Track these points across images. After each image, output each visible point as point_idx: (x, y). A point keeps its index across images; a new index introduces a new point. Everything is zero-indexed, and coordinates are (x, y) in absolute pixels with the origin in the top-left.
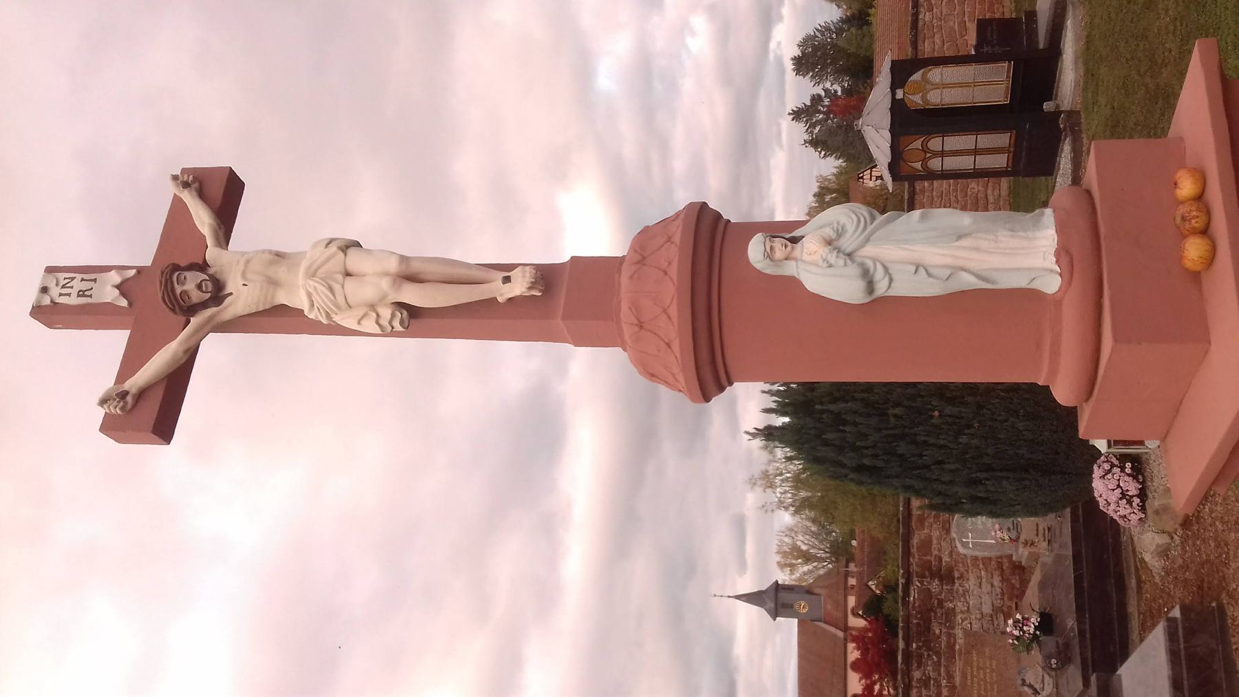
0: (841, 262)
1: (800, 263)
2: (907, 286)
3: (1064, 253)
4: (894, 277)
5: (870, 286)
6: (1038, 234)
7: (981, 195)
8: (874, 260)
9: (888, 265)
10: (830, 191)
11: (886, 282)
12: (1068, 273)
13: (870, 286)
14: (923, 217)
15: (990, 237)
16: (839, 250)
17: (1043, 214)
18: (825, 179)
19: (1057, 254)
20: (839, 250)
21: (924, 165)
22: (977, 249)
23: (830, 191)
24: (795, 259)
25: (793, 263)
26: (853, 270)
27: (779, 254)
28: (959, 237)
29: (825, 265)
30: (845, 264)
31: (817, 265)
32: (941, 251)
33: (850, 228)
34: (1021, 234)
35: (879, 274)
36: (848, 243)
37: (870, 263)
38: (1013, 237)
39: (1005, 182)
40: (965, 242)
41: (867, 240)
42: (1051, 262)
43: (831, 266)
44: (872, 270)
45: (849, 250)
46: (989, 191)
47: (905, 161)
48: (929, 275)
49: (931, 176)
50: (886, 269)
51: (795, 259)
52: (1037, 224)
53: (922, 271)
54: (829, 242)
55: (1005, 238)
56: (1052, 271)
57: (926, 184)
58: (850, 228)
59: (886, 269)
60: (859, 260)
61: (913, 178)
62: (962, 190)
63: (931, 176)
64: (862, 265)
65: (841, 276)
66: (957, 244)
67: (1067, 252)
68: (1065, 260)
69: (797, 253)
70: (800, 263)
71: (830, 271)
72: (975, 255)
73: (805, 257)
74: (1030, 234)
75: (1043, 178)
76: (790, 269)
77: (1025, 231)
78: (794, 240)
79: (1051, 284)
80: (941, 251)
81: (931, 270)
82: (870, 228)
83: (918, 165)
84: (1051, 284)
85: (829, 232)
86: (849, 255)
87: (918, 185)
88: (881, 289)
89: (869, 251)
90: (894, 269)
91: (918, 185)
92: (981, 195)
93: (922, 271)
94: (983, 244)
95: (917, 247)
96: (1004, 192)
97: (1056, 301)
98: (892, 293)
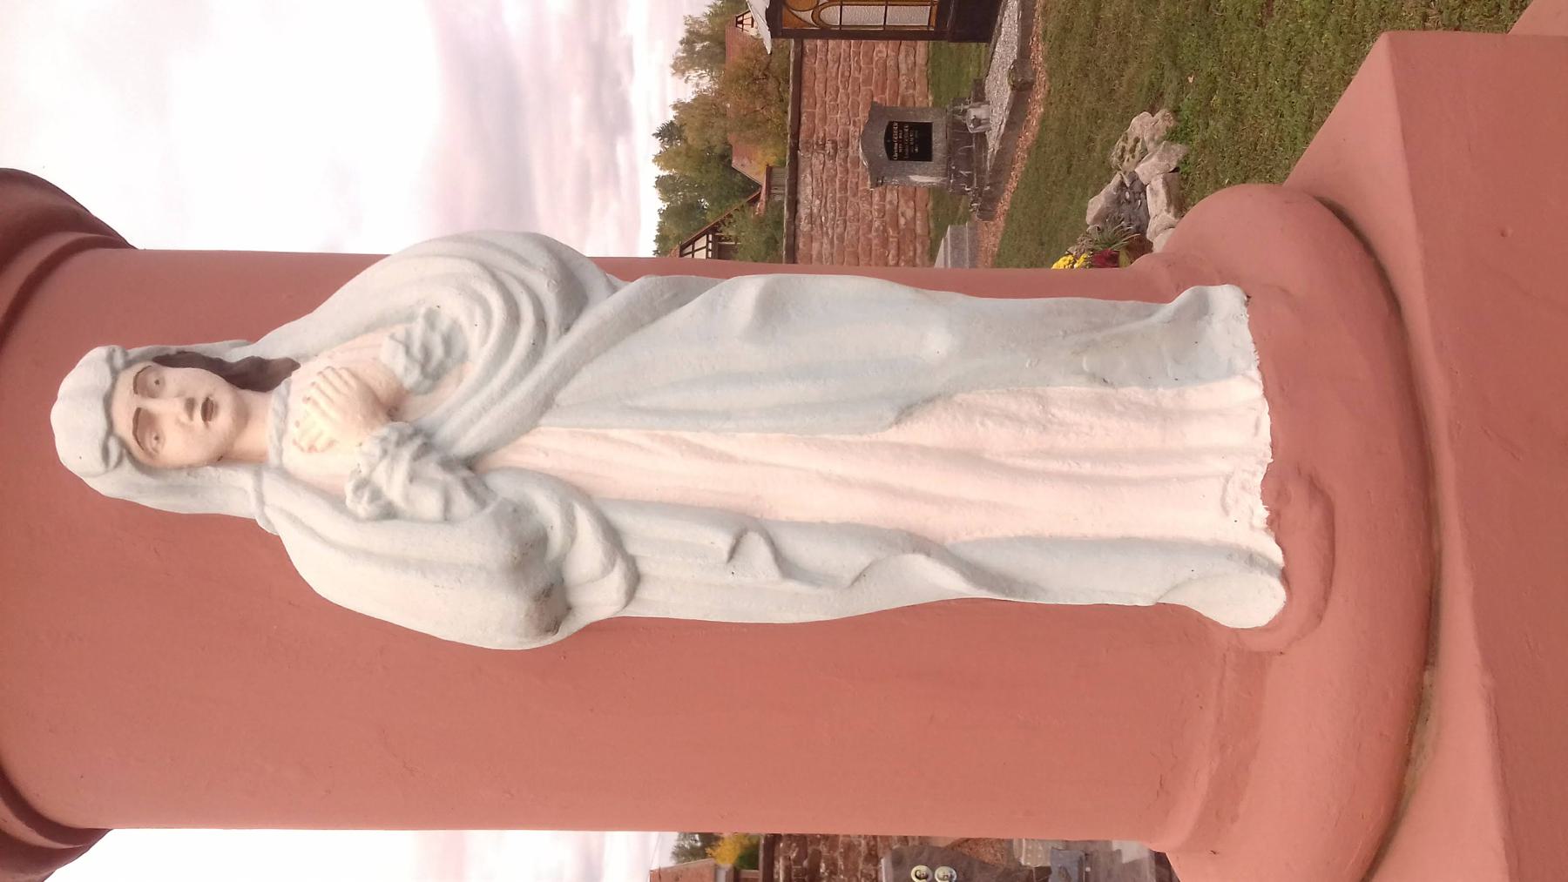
0: (429, 503)
1: (270, 482)
2: (691, 584)
3: (1295, 485)
4: (644, 567)
5: (552, 600)
6: (1197, 396)
7: (890, 63)
8: (572, 492)
9: (624, 520)
10: (702, 38)
11: (616, 580)
12: (1315, 567)
13: (552, 600)
14: (769, 310)
15: (1028, 407)
16: (426, 443)
17: (1202, 309)
18: (696, 21)
19: (1276, 490)
20: (426, 443)
21: (816, 16)
22: (970, 459)
23: (702, 38)
24: (256, 462)
25: (242, 479)
26: (478, 543)
27: (179, 439)
28: (906, 411)
29: (363, 507)
30: (447, 516)
31: (334, 500)
32: (838, 467)
33: (479, 345)
34: (1135, 392)
35: (586, 557)
36: (463, 415)
37: (548, 509)
38: (1103, 405)
39: (921, 46)
40: (925, 431)
41: (544, 404)
42: (1247, 521)
43: (389, 513)
44: (557, 538)
45: (467, 444)
46: (901, 57)
47: (788, 7)
48: (785, 565)
49: (826, 32)
50: (613, 537)
51: (256, 462)
52: (1186, 354)
53: (758, 550)
54: (389, 407)
55: (1079, 417)
56: (1252, 559)
57: (819, 42)
58: (479, 345)
59: (613, 537)
60: (503, 486)
61: (801, 34)
62: (866, 54)
63: (826, 32)
64: (517, 516)
65: (424, 567)
66: (894, 435)
67: (1316, 489)
68: (1303, 514)
69: (261, 435)
70: (269, 480)
71: (383, 538)
72: (969, 487)
73: (294, 459)
74: (1166, 395)
75: (974, 45)
76: (234, 494)
77: (1147, 381)
78: (258, 377)
79: (1251, 603)
80: (838, 467)
81: (802, 550)
82: (556, 352)
83: (807, 16)
84: (1251, 603)
85: (390, 362)
86: (472, 467)
87: (808, 44)
88: (600, 598)
89: (554, 447)
90: (640, 530)
91: (808, 44)
92: (890, 63)
93: (758, 550)
94: (997, 438)
95: (742, 443)
96: (921, 60)
97: (1249, 656)
98: (634, 611)
